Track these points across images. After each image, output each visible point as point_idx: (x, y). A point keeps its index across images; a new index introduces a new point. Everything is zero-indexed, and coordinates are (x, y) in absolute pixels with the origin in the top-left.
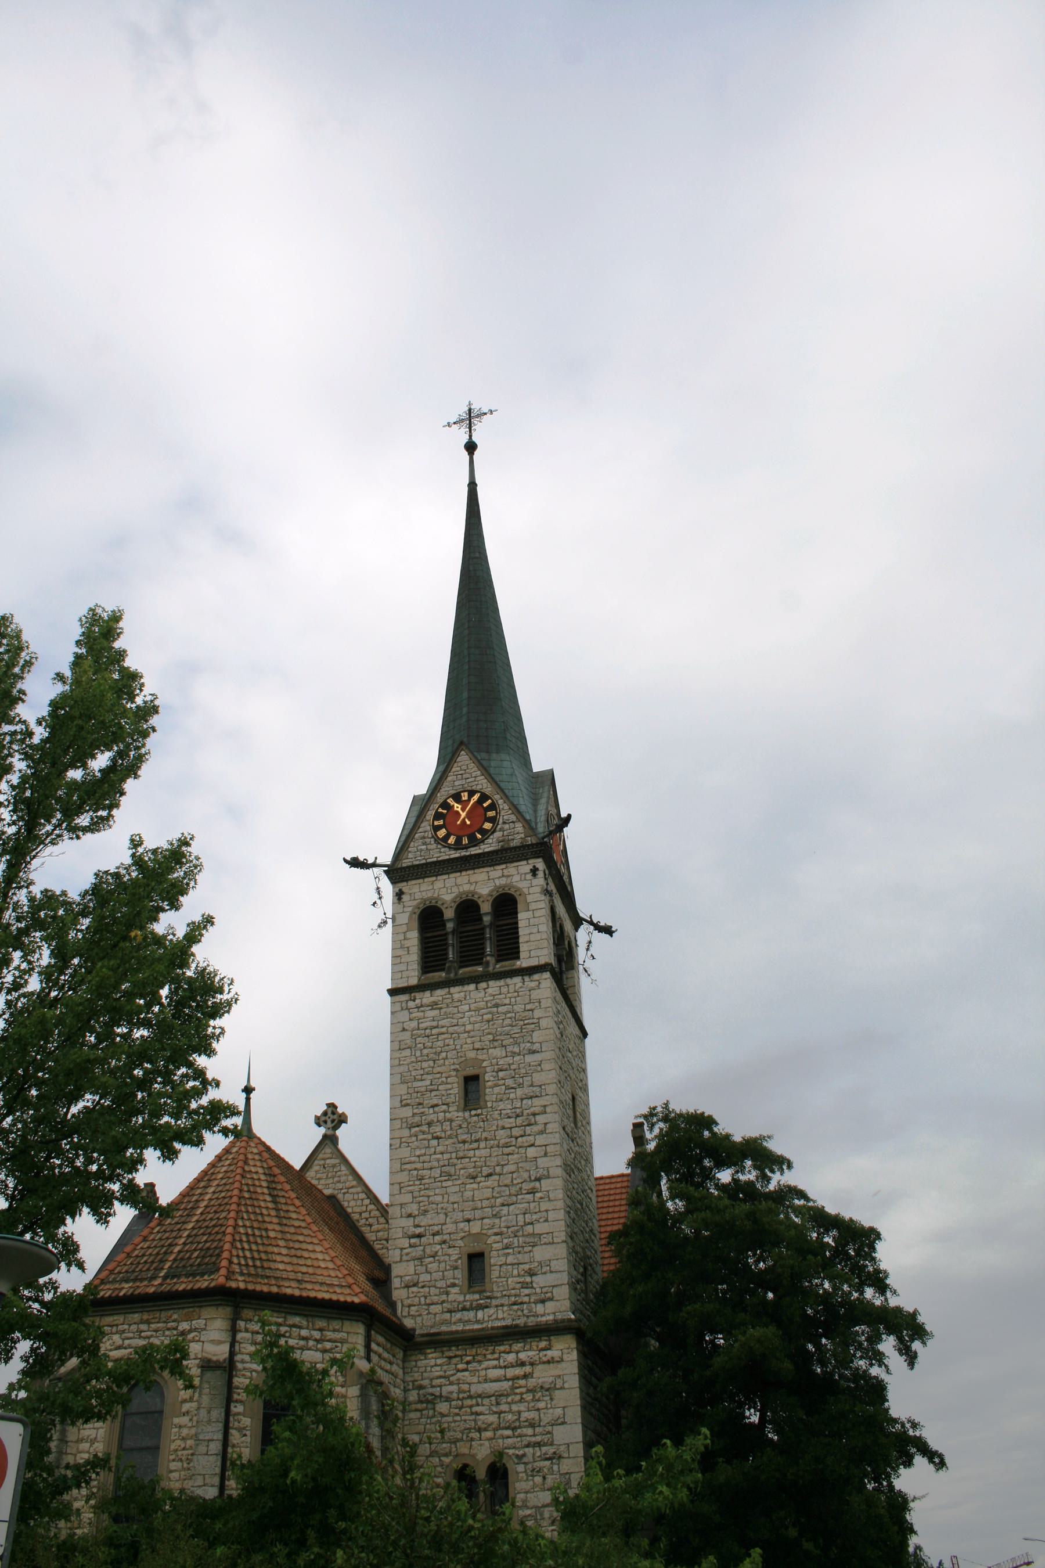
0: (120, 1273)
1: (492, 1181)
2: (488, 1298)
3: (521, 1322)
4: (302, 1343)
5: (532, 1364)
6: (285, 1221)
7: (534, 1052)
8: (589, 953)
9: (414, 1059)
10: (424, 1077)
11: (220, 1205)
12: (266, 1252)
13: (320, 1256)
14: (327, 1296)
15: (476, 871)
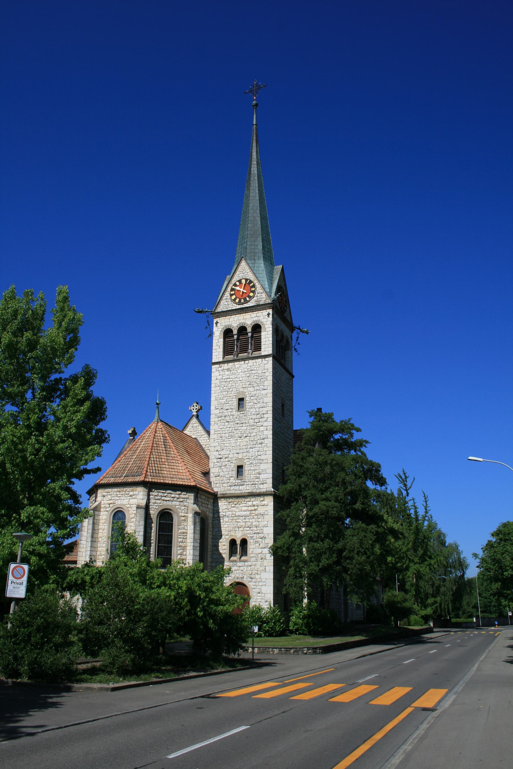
0: (110, 474)
1: (247, 439)
2: (244, 482)
3: (254, 491)
4: (172, 499)
5: (257, 506)
6: (168, 455)
7: (264, 389)
8: (297, 342)
9: (220, 391)
10: (224, 398)
11: (145, 449)
12: (160, 467)
13: (180, 468)
14: (181, 483)
15: (246, 314)
